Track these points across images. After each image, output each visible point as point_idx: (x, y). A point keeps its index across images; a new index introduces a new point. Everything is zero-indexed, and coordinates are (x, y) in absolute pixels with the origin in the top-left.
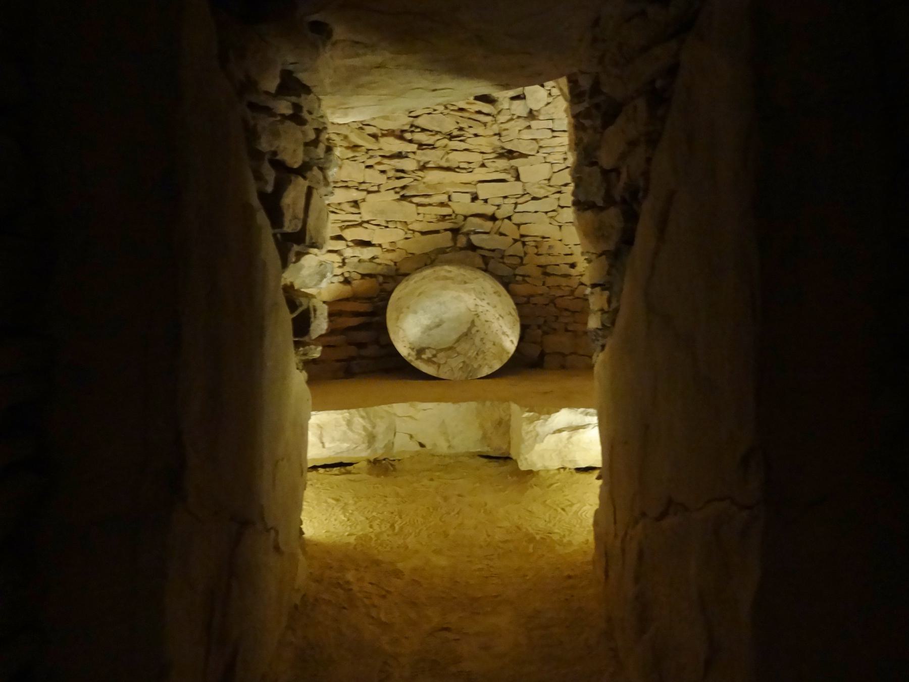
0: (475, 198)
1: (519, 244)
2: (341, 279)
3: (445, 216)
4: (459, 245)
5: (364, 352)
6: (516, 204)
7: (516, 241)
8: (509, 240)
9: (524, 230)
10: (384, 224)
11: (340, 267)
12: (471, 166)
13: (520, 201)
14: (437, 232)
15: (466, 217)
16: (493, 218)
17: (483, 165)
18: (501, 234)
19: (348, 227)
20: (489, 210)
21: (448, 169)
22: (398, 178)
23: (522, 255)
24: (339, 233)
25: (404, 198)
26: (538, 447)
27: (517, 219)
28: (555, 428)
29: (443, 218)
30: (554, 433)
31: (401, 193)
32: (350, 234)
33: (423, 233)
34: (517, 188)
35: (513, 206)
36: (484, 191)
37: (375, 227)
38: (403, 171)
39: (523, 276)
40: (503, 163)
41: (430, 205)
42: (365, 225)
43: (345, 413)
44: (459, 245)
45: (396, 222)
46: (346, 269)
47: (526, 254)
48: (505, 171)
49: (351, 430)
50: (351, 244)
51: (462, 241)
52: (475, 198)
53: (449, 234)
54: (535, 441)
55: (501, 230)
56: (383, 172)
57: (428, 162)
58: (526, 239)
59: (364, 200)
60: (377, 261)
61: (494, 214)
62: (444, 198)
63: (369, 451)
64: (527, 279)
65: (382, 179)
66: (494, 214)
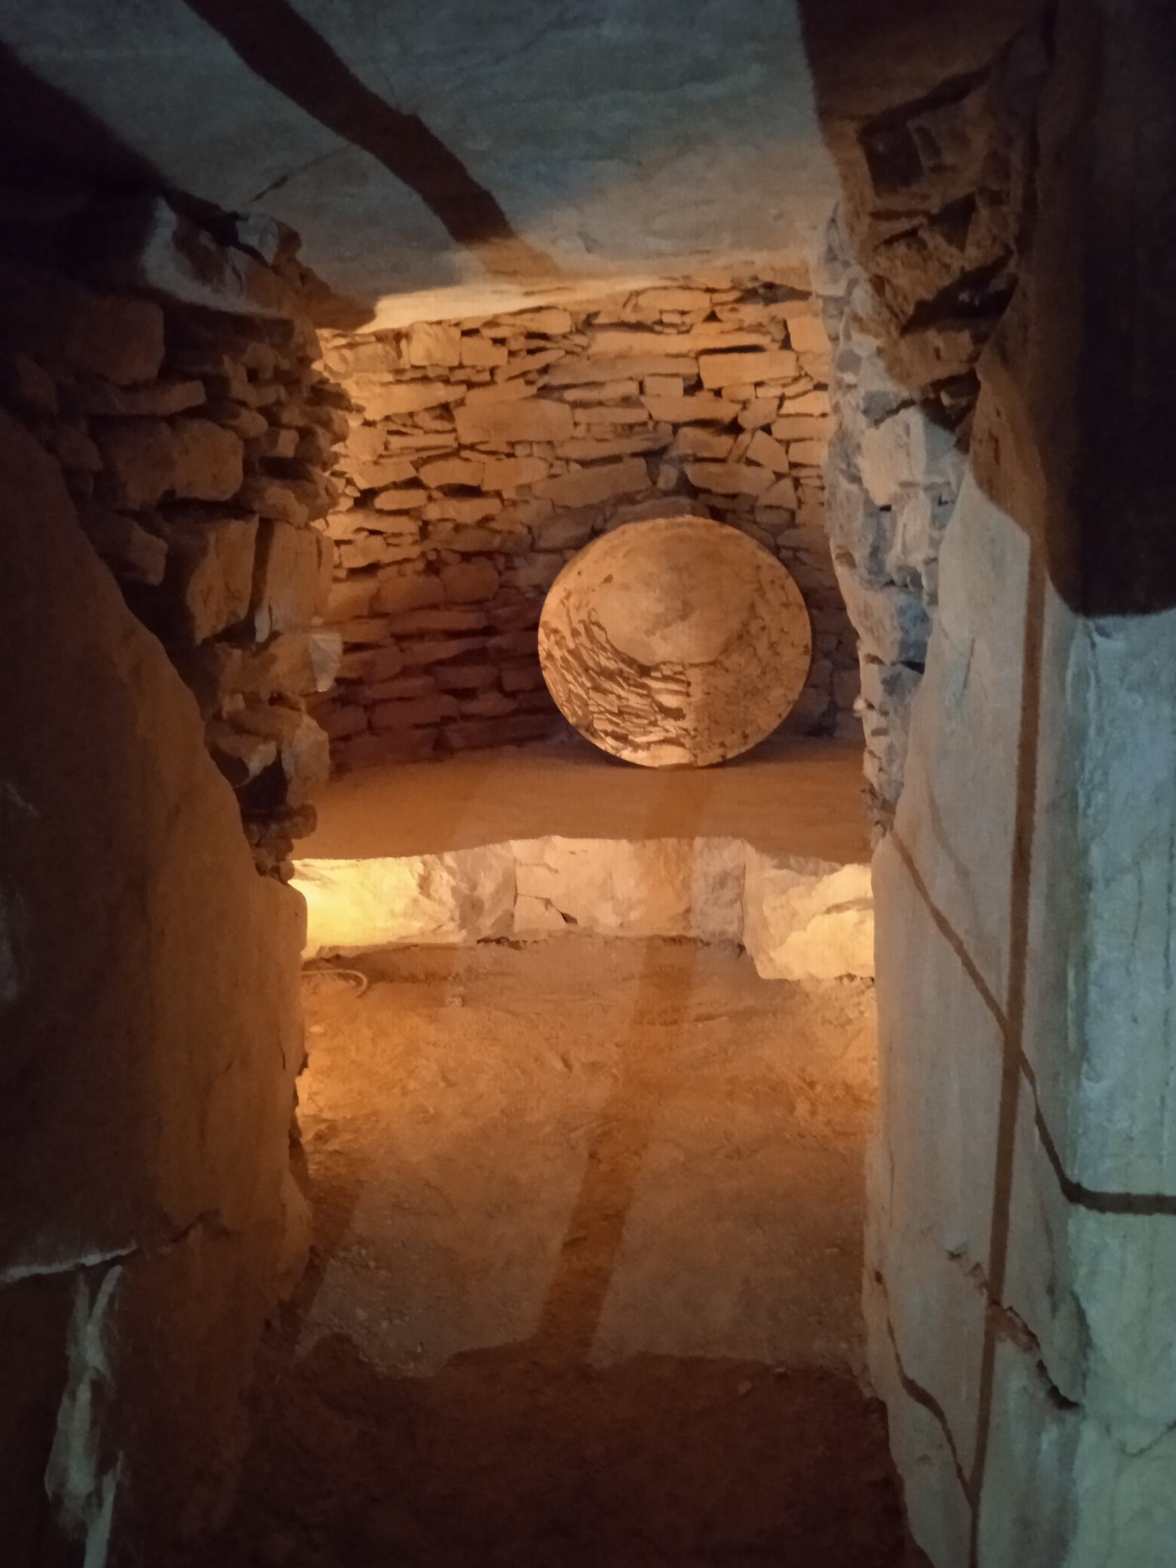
0: (694, 386)
1: (787, 484)
2: (420, 565)
3: (631, 426)
4: (662, 484)
5: (473, 707)
6: (782, 399)
7: (779, 476)
8: (767, 475)
9: (797, 453)
10: (507, 450)
11: (415, 543)
12: (688, 319)
13: (790, 391)
14: (616, 459)
15: (676, 427)
16: (734, 428)
17: (712, 317)
18: (751, 463)
19: (428, 460)
20: (724, 411)
21: (638, 327)
22: (531, 352)
23: (793, 505)
24: (410, 473)
25: (545, 391)
26: (795, 938)
27: (781, 429)
28: (831, 902)
29: (630, 428)
30: (828, 911)
31: (540, 383)
32: (432, 475)
33: (584, 464)
34: (786, 365)
35: (776, 402)
36: (714, 372)
37: (484, 457)
38: (544, 336)
39: (795, 550)
40: (752, 313)
41: (601, 403)
42: (465, 454)
43: (416, 864)
44: (662, 484)
45: (531, 443)
46: (428, 545)
47: (800, 502)
48: (758, 328)
49: (428, 896)
50: (436, 494)
51: (668, 476)
52: (694, 386)
53: (641, 463)
54: (791, 928)
55: (750, 454)
56: (499, 342)
57: (596, 314)
58: (803, 473)
59: (461, 402)
60: (494, 525)
61: (735, 420)
62: (632, 388)
63: (464, 933)
64: (801, 555)
65: (499, 356)
66: (735, 420)
